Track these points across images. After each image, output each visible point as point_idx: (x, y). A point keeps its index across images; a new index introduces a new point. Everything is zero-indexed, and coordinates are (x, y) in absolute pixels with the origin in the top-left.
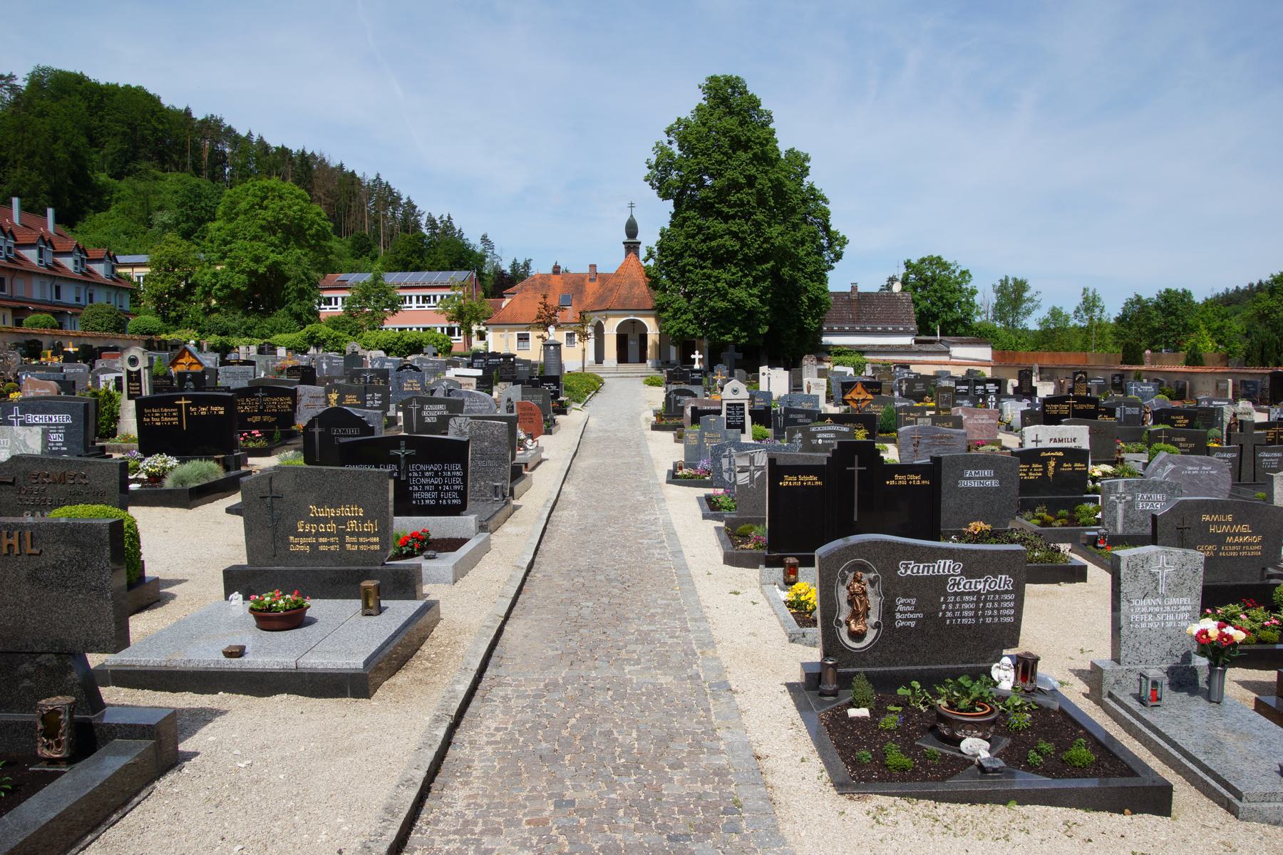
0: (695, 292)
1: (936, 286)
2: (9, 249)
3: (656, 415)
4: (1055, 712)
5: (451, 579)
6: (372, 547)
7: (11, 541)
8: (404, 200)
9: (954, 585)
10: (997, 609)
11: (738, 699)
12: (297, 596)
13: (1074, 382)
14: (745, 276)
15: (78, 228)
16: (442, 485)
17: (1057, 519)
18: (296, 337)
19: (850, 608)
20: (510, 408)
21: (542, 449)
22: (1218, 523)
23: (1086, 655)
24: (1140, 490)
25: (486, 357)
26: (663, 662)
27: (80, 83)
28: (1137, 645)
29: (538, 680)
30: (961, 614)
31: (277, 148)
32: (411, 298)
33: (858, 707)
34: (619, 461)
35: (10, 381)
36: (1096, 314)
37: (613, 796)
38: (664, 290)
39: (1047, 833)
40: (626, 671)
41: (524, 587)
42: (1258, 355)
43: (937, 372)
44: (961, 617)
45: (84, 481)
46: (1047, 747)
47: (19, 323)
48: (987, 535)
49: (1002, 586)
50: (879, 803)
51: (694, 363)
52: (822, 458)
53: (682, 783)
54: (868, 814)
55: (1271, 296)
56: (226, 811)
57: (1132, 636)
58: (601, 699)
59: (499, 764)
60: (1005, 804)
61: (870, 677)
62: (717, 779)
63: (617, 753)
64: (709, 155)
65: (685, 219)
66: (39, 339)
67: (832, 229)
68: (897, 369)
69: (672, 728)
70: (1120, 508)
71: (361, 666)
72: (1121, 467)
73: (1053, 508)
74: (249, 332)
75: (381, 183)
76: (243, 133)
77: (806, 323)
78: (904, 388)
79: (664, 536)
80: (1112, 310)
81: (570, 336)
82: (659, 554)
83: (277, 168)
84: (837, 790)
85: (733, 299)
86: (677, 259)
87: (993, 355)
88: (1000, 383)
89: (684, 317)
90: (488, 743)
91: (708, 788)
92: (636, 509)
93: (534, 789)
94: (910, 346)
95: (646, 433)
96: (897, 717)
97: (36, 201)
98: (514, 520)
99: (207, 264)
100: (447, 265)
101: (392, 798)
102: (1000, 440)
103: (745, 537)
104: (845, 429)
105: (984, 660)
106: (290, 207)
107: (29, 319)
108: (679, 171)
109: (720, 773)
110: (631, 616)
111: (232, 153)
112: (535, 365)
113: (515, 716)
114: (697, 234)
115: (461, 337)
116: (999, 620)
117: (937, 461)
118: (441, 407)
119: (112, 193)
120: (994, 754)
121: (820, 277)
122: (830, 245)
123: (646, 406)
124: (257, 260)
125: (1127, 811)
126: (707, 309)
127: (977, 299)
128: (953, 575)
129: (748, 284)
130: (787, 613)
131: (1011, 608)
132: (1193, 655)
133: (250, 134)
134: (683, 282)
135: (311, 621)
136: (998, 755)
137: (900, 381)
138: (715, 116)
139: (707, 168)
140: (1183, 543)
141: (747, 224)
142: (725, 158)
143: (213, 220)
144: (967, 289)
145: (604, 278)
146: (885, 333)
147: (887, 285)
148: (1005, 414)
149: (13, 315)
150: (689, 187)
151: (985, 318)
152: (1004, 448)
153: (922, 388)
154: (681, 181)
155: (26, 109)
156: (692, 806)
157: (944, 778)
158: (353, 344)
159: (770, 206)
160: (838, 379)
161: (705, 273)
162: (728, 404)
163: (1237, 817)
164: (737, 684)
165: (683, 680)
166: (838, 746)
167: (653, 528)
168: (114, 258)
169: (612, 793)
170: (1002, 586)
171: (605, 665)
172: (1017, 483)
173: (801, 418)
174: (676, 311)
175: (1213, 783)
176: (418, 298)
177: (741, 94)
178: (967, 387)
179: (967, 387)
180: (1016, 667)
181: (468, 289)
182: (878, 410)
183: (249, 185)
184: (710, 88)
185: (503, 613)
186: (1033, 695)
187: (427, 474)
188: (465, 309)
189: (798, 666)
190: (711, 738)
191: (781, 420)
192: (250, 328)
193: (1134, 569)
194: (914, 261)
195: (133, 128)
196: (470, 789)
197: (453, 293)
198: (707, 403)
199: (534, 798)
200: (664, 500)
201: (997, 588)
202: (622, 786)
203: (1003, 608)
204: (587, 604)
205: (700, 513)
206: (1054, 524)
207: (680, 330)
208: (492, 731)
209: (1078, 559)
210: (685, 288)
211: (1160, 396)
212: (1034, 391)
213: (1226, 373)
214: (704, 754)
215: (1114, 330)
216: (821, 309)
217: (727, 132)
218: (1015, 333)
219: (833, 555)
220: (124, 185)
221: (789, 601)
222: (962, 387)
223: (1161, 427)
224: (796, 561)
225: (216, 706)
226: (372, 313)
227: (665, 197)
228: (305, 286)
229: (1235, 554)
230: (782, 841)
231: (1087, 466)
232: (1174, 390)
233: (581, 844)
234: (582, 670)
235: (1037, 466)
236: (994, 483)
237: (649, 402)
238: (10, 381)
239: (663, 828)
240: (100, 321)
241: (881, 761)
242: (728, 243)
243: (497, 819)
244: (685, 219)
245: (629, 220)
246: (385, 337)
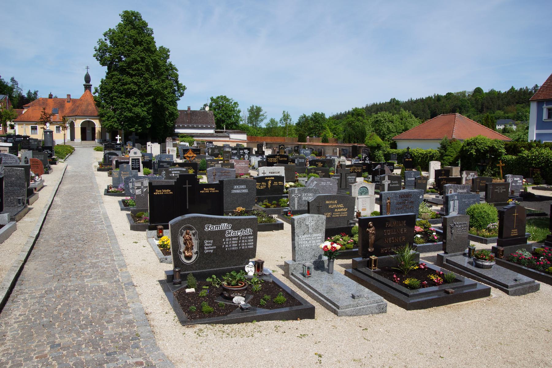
0: (117, 109)
1: (224, 108)
3: (99, 164)
4: (271, 283)
9: (228, 234)
10: (231, 241)
11: (137, 289)
13: (280, 149)
14: (140, 102)
17: (272, 205)
19: (185, 246)
20: (27, 162)
21: (44, 181)
22: (332, 204)
23: (283, 259)
24: (303, 192)
25: (14, 137)
26: (103, 276)
28: (302, 254)
29: (41, 289)
30: (232, 246)
33: (190, 288)
34: (81, 186)
36: (288, 121)
37: (80, 339)
38: (103, 107)
39: (268, 331)
40: (85, 281)
41: (35, 246)
42: (348, 139)
43: (224, 145)
44: (232, 247)
46: (267, 297)
48: (243, 212)
49: (248, 233)
50: (199, 328)
51: (117, 141)
52: (172, 182)
53: (112, 329)
54: (195, 333)
55: (352, 116)
57: (300, 250)
58: (73, 295)
59: (21, 332)
60: (251, 322)
61: (194, 275)
62: (128, 325)
64: (124, 47)
65: (113, 75)
67: (179, 82)
68: (208, 144)
69: (107, 305)
70: (296, 199)
72: (297, 183)
73: (270, 201)
77: (167, 124)
78: (210, 152)
79: (103, 219)
80: (294, 120)
81: (58, 128)
82: (100, 227)
84: (182, 324)
85: (135, 112)
86: (109, 93)
87: (247, 138)
88: (250, 149)
89: (113, 120)
90: (15, 322)
91: (124, 330)
92: (89, 207)
93: (40, 341)
94: (213, 134)
95: (94, 172)
96: (206, 291)
98: (29, 215)
102: (250, 173)
103: (140, 218)
104: (184, 169)
105: (242, 264)
108: (110, 53)
109: (130, 322)
110: (88, 256)
112: (40, 141)
113: (30, 308)
114: (118, 82)
116: (247, 247)
117: (221, 182)
120: (247, 302)
121: (174, 104)
122: (179, 89)
123: (95, 160)
125: (299, 319)
126: (123, 116)
127: (241, 114)
128: (228, 230)
129: (141, 105)
130: (159, 250)
131: (252, 242)
132: (323, 256)
134: (112, 104)
136: (249, 303)
137: (208, 149)
138: (127, 29)
139: (123, 53)
140: (319, 212)
141: (141, 79)
142: (131, 49)
144: (237, 110)
145: (74, 101)
146: (202, 128)
147: (203, 108)
148: (252, 162)
150: (115, 61)
151: (244, 122)
152: (251, 176)
153: (218, 152)
154: (111, 58)
156: (117, 339)
157: (227, 314)
159: (152, 71)
160: (181, 148)
161: (122, 101)
162: (132, 159)
163: (337, 316)
164: (137, 282)
165: (112, 283)
166: (182, 305)
167: (98, 215)
169: (79, 338)
170: (248, 233)
171: (75, 279)
172: (255, 191)
173: (165, 165)
175: (330, 304)
177: (139, 20)
178: (236, 151)
179: (236, 151)
180: (255, 266)
181: (4, 104)
182: (199, 161)
184: (124, 16)
185: (23, 259)
186: (262, 277)
189: (164, 273)
190: (125, 307)
191: (156, 166)
193: (300, 223)
194: (215, 98)
196: (5, 347)
198: (123, 158)
199: (40, 345)
200: (103, 203)
201: (246, 234)
202: (84, 334)
203: (249, 242)
204: (66, 252)
205: (119, 208)
206: (271, 207)
207: (111, 126)
208: (17, 316)
209: (280, 221)
210: (113, 107)
211: (312, 155)
212: (263, 153)
213: (336, 146)
214: (122, 315)
215: (295, 128)
216: (174, 118)
218: (256, 129)
219: (177, 223)
221: (159, 245)
222: (234, 151)
223: (312, 167)
224: (162, 227)
227: (103, 64)
229: (338, 216)
230: (158, 349)
231: (283, 183)
232: (318, 152)
233: (64, 364)
234: (64, 282)
235: (264, 183)
236: (246, 191)
237: (97, 158)
239: (103, 350)
241: (200, 310)
242: (132, 87)
243: (20, 359)
244: (113, 75)
245: (86, 74)
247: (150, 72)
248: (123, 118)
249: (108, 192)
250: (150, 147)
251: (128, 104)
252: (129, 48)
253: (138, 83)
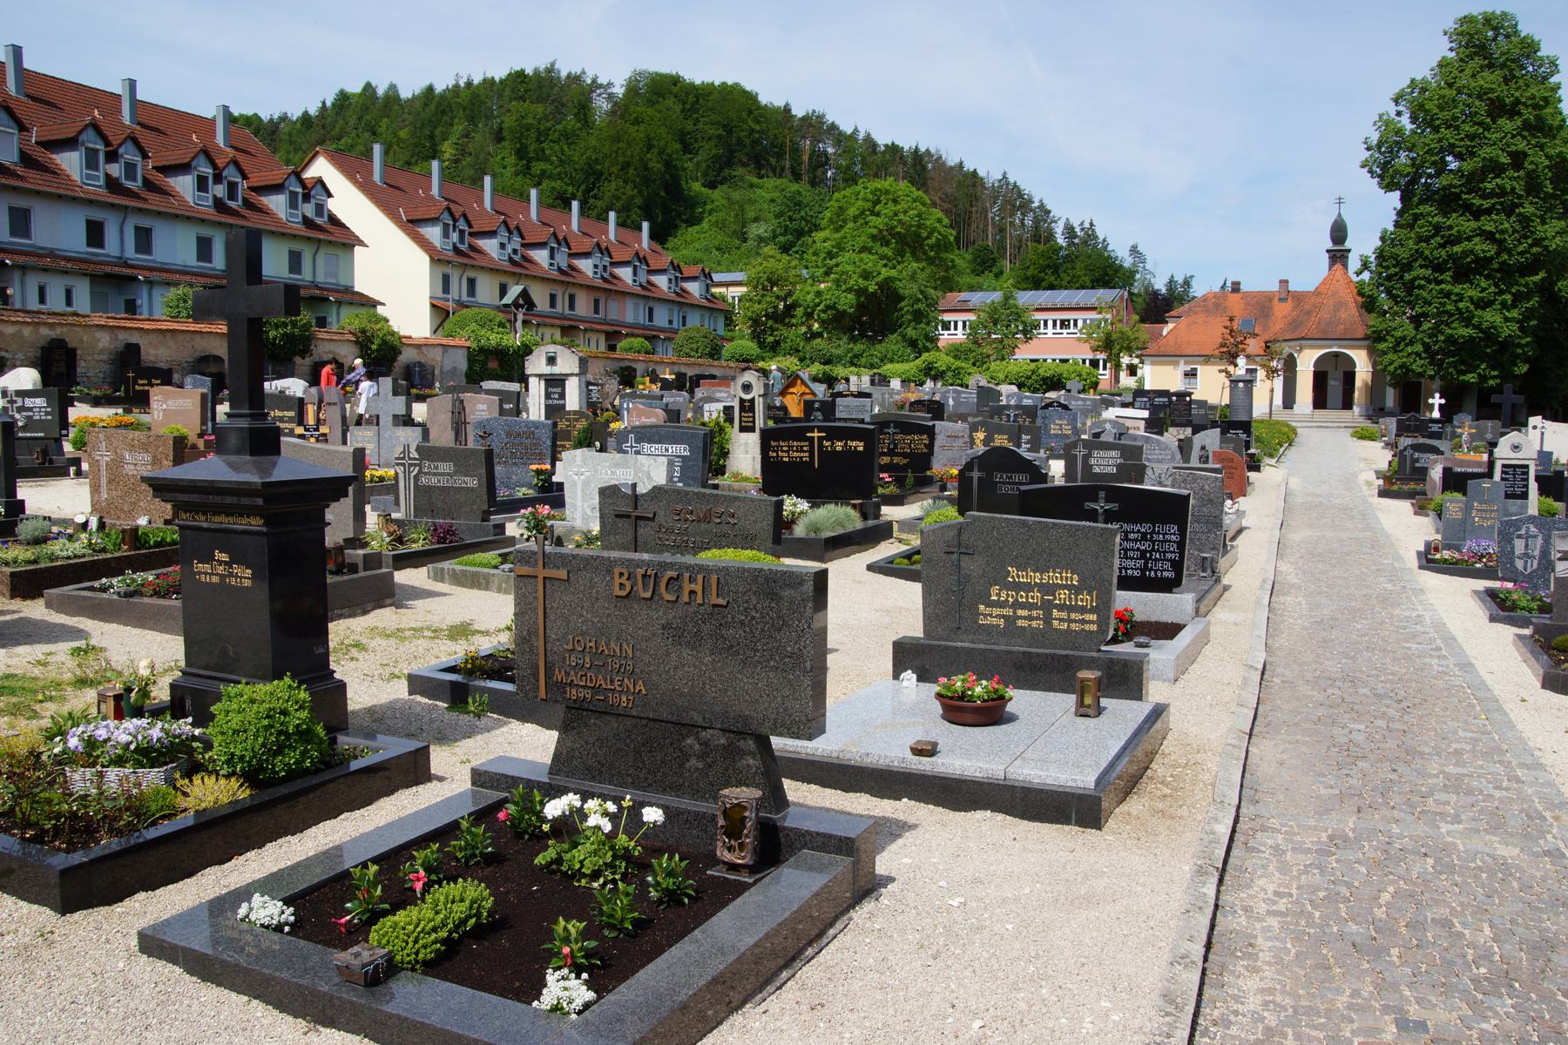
0: (1425, 315)
2: (605, 267)
5: (1172, 676)
6: (1087, 627)
7: (693, 586)
8: (1036, 204)
12: (998, 683)
14: (1501, 292)
15: (669, 244)
16: (1150, 552)
18: (911, 367)
26: (1497, 825)
27: (675, 85)
31: (886, 146)
32: (1046, 322)
35: (607, 410)
45: (732, 521)
47: (612, 348)
56: (949, 967)
63: (1470, 958)
64: (1457, 128)
66: (634, 365)
71: (1092, 786)
74: (855, 361)
75: (1008, 184)
76: (847, 129)
83: (886, 169)
89: (1409, 349)
95: (1370, 500)
97: (628, 217)
99: (810, 281)
100: (1088, 283)
101: (1168, 981)
106: (905, 212)
107: (623, 344)
108: (1410, 151)
110: (1427, 750)
111: (835, 154)
112: (1213, 408)
113: (1299, 878)
114: (1433, 236)
115: (1107, 372)
118: (1114, 453)
119: (705, 203)
124: (866, 275)
126: (1441, 338)
129: (1504, 305)
133: (856, 129)
134: (1409, 303)
135: (1011, 719)
138: (1466, 72)
139: (1452, 146)
142: (1481, 130)
143: (817, 228)
145: (1299, 297)
149: (607, 340)
155: (622, 117)
158: (978, 377)
161: (1442, 290)
162: (1504, 466)
167: (1419, 628)
168: (708, 276)
171: (1409, 818)
174: (1398, 341)
176: (1055, 322)
177: (1507, 36)
183: (859, 188)
184: (1461, 34)
187: (1132, 536)
188: (1114, 336)
192: (856, 356)
195: (728, 129)
197: (1099, 316)
207: (1403, 366)
208: (1270, 895)
217: (1485, 93)
220: (718, 195)
225: (902, 817)
226: (1001, 341)
227: (1389, 187)
228: (921, 306)
238: (607, 410)
240: (695, 346)
244: (1416, 217)
246: (1016, 369)
249: (1429, 560)
250: (1538, 432)
252: (1472, 130)
253: (1497, 236)
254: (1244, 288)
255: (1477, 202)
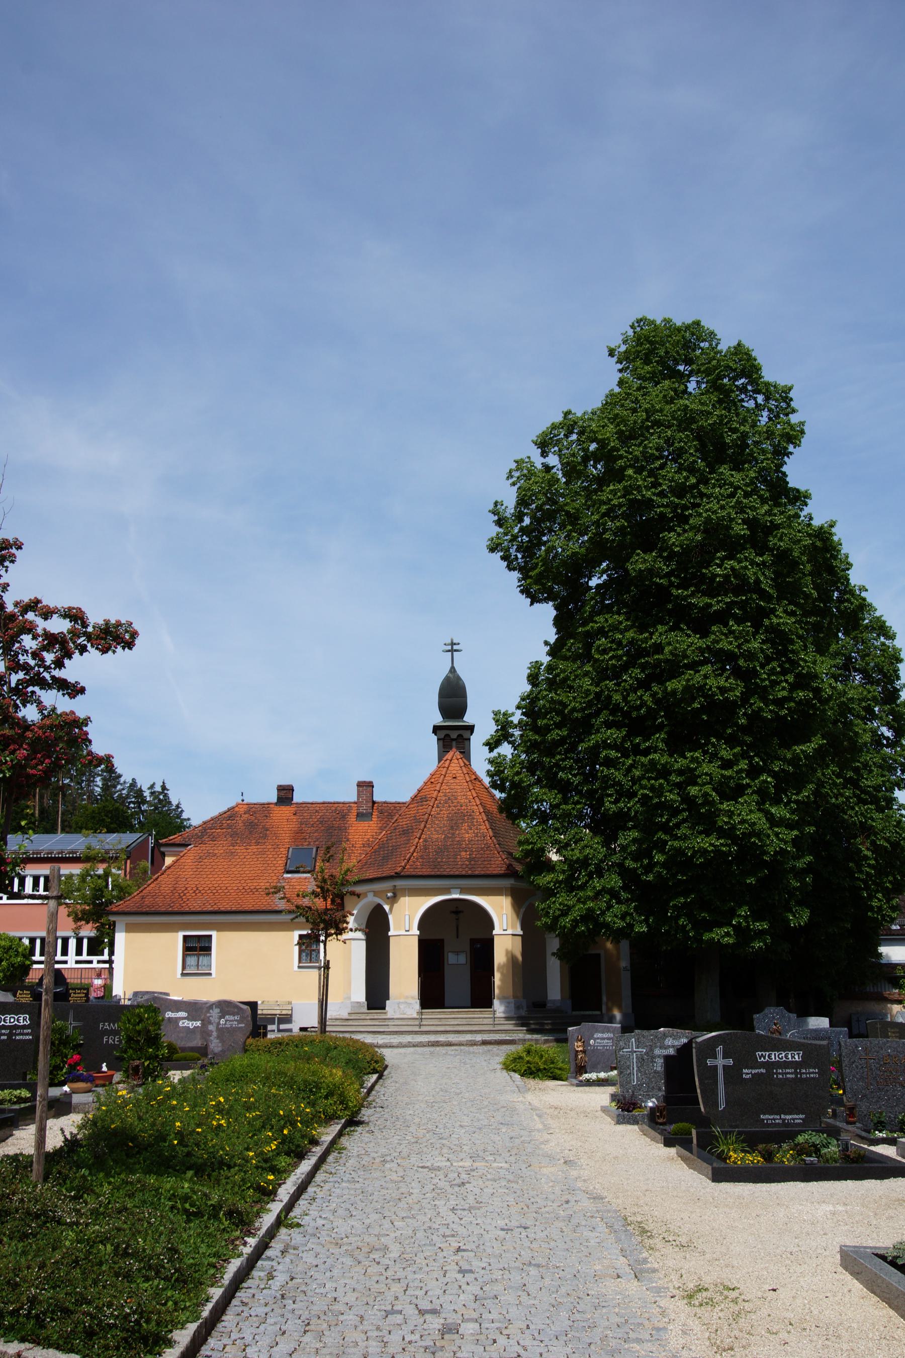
14: (753, 772)
77: (871, 908)
89: (597, 884)
114: (625, 668)
145: (389, 811)
207: (588, 917)
244: (590, 637)
247: (796, 605)
248: (664, 865)
251: (692, 780)
252: (680, 478)
254: (297, 798)
255: (700, 601)
